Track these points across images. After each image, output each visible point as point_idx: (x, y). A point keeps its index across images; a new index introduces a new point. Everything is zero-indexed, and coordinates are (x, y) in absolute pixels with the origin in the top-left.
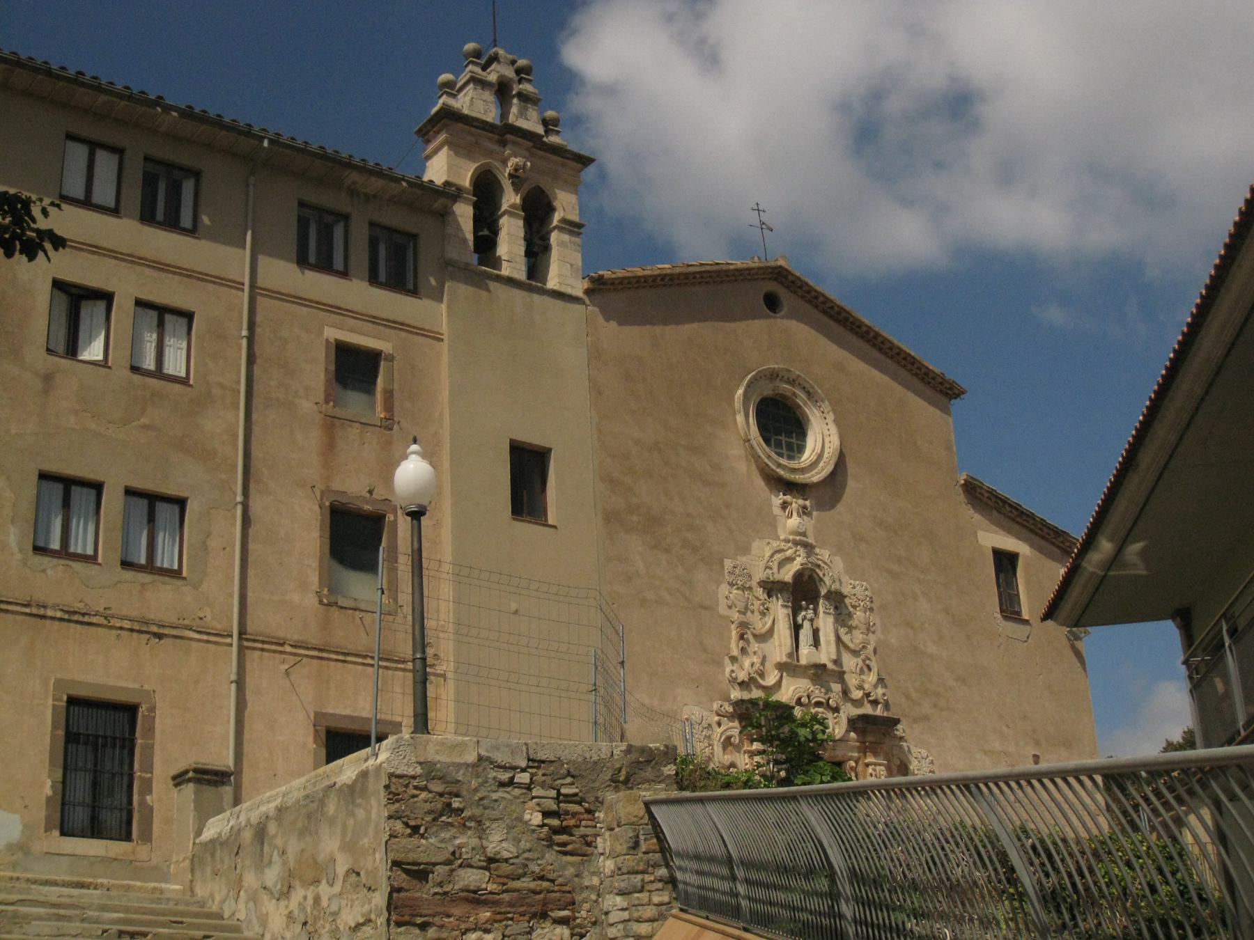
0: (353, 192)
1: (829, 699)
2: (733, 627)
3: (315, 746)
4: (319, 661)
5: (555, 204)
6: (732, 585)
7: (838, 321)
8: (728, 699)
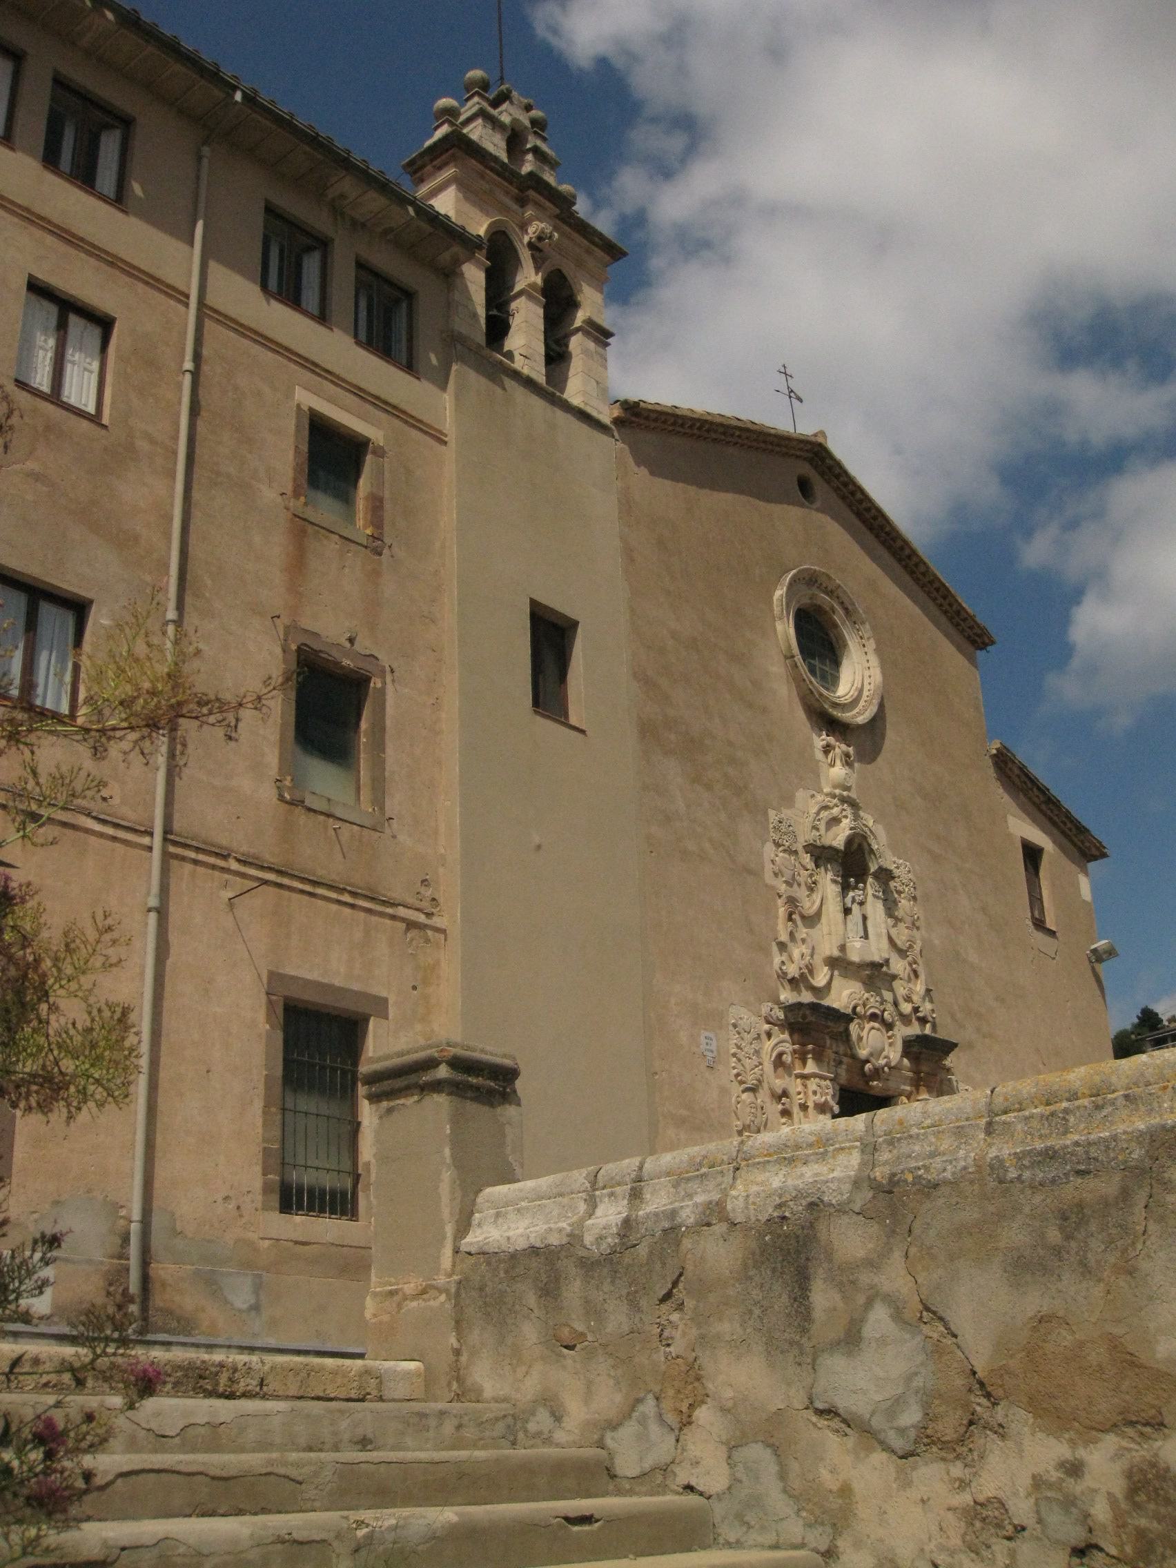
0: (336, 210)
1: (884, 1010)
2: (780, 902)
3: (268, 1027)
4: (277, 890)
5: (579, 298)
6: (778, 845)
7: (871, 529)
8: (777, 1002)
